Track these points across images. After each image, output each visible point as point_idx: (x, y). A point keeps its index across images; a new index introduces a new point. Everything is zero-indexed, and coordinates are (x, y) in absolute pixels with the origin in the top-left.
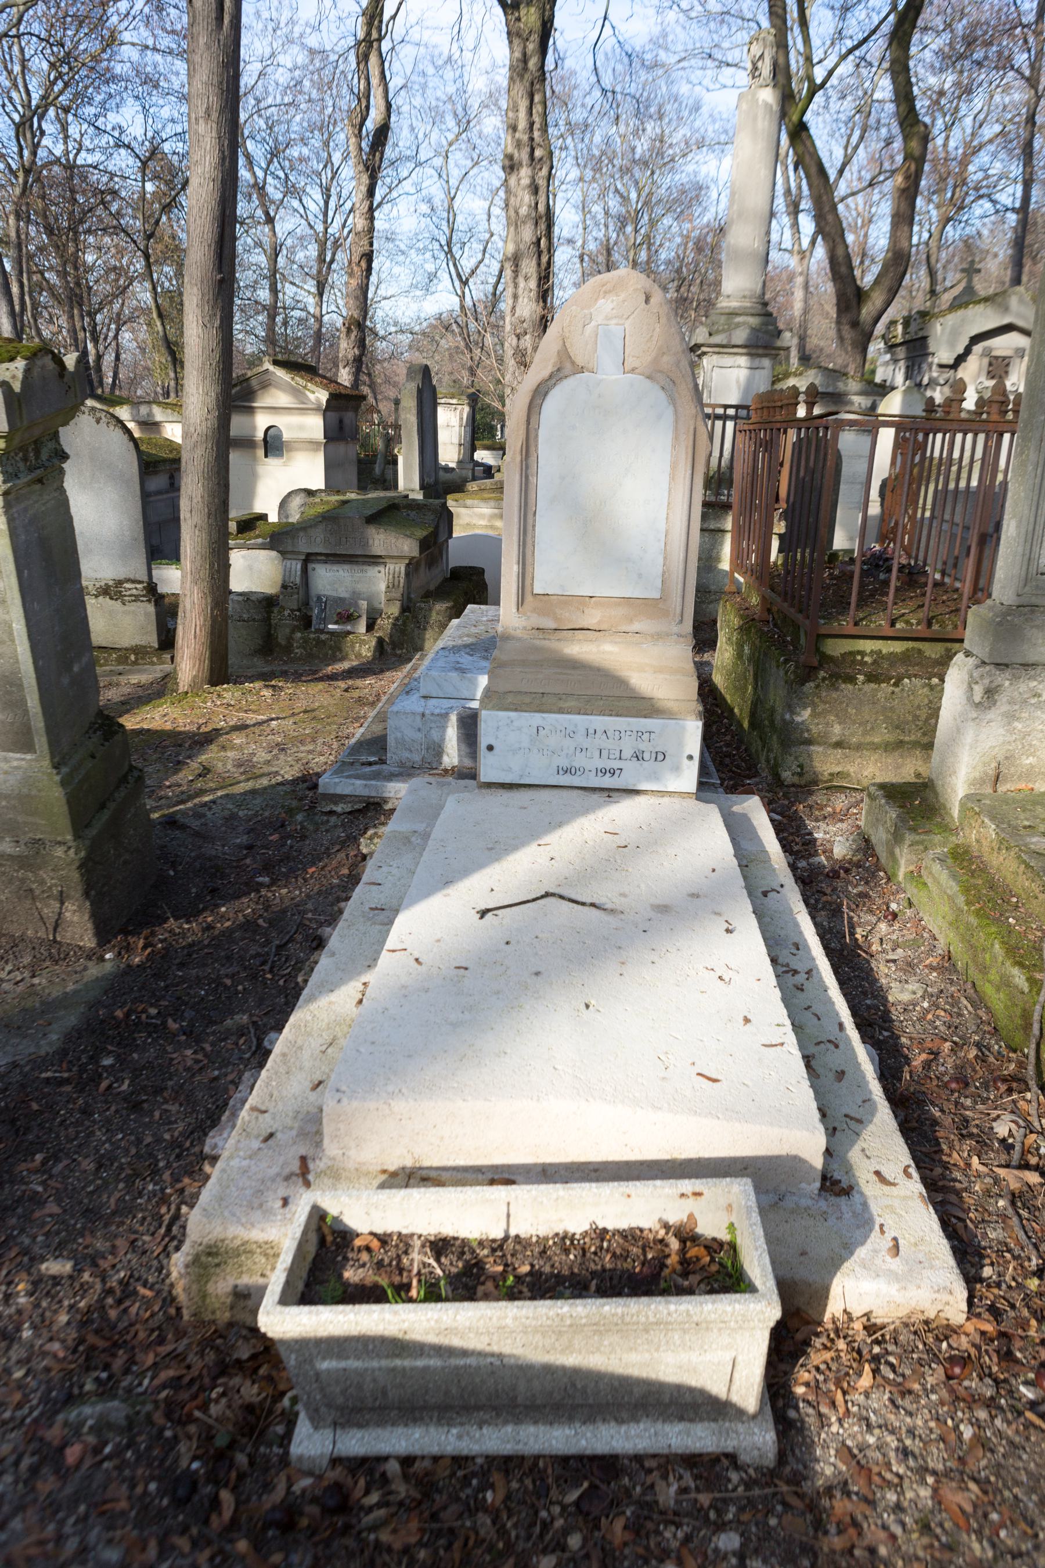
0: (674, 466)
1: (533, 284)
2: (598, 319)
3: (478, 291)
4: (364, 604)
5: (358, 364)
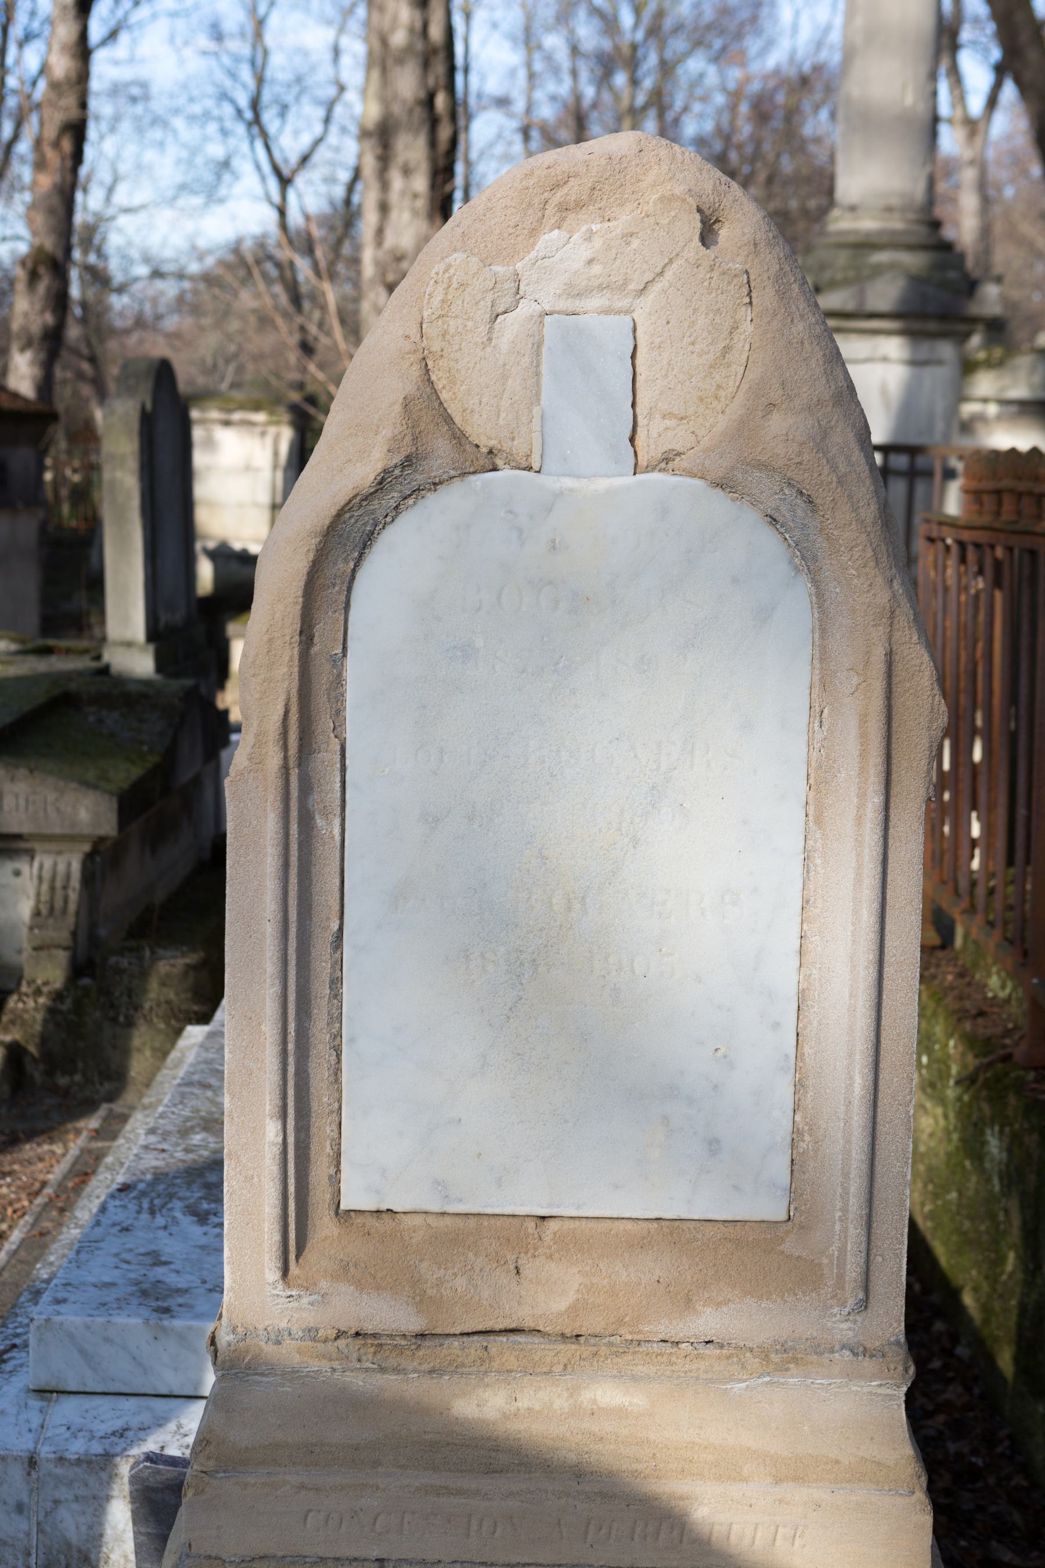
0: (819, 780)
1: (421, 183)
2: (544, 293)
3: (311, 197)
5: (52, 344)
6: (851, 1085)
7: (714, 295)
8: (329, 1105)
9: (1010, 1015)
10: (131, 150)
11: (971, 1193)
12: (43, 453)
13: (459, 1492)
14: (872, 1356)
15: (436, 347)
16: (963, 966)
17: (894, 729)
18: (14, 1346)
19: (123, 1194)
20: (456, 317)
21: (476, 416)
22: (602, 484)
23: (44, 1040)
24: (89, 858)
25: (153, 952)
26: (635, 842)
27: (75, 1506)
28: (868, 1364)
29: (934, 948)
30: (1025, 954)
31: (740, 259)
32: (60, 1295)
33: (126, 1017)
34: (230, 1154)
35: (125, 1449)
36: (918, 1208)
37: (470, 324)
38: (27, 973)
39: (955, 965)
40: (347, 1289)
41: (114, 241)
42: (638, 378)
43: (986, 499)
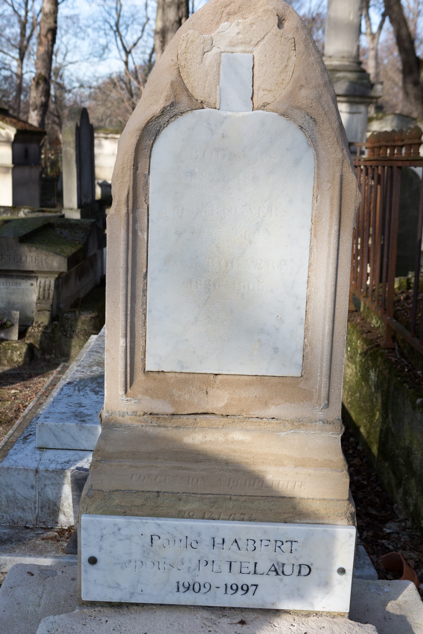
0: (316, 221)
2: (221, 45)
3: (138, 59)
4: (17, 314)
5: (44, 108)
6: (324, 329)
7: (282, 46)
8: (142, 334)
9: (379, 332)
10: (74, 40)
11: (364, 393)
12: (41, 148)
13: (186, 469)
14: (330, 424)
15: (183, 63)
16: (363, 317)
17: (342, 203)
18: (31, 434)
19: (69, 385)
20: (190, 53)
21: (197, 89)
22: (241, 114)
23: (41, 343)
24: (57, 280)
25: (79, 313)
26: (251, 242)
27: (52, 487)
28: (328, 427)
29: (353, 311)
30: (385, 310)
31: (292, 33)
32: (47, 416)
33: (70, 335)
34: (107, 350)
35: (69, 467)
36: (345, 400)
37: (195, 56)
38: (36, 319)
39: (361, 317)
40: (147, 398)
41: (66, 73)
42: (255, 76)
43: (376, 150)
